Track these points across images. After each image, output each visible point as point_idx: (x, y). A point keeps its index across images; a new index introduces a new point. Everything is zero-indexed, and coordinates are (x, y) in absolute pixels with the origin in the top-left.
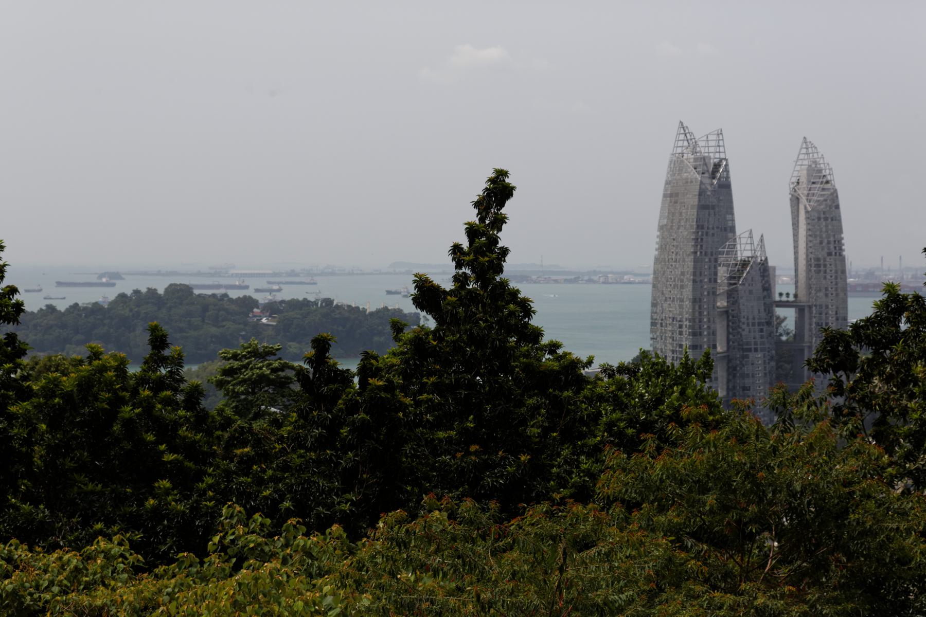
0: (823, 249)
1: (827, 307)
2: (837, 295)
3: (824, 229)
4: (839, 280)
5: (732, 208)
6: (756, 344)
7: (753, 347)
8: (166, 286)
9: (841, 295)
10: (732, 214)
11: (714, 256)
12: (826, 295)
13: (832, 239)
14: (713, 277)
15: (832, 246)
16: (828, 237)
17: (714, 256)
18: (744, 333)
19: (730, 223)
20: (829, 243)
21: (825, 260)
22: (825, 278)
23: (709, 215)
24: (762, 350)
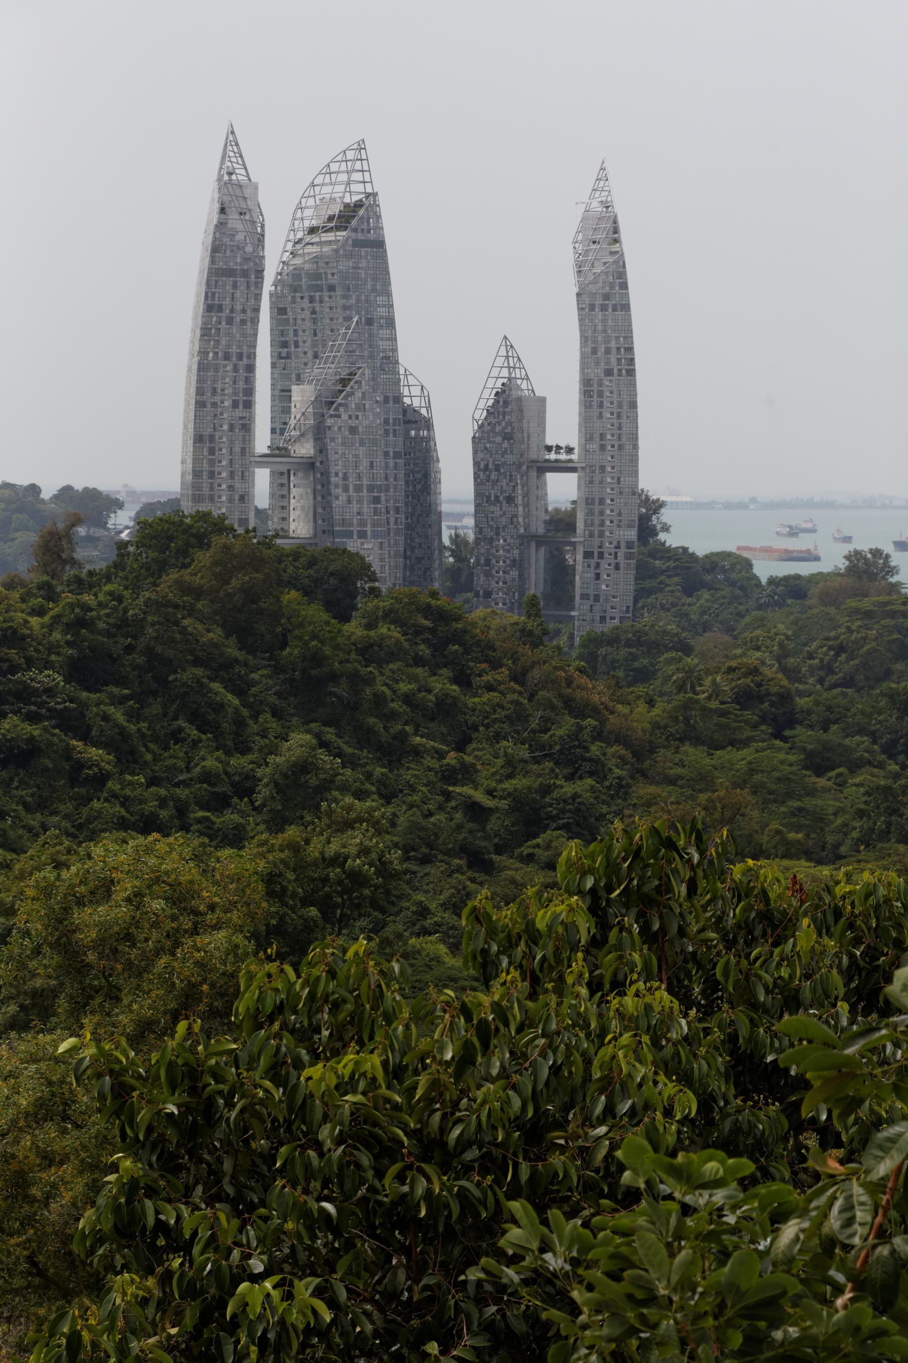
0: (597, 363)
1: (603, 468)
2: (620, 448)
3: (600, 328)
4: (624, 420)
5: (387, 282)
6: (362, 523)
7: (355, 529)
8: (91, 486)
9: (628, 447)
10: (389, 294)
11: (245, 361)
12: (602, 448)
13: (613, 344)
14: (241, 398)
15: (613, 360)
16: (607, 341)
17: (245, 361)
18: (335, 503)
19: (382, 311)
20: (608, 351)
21: (600, 384)
22: (601, 416)
23: (235, 286)
24: (375, 535)
